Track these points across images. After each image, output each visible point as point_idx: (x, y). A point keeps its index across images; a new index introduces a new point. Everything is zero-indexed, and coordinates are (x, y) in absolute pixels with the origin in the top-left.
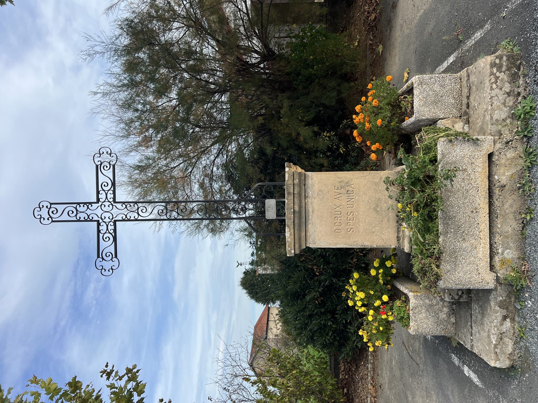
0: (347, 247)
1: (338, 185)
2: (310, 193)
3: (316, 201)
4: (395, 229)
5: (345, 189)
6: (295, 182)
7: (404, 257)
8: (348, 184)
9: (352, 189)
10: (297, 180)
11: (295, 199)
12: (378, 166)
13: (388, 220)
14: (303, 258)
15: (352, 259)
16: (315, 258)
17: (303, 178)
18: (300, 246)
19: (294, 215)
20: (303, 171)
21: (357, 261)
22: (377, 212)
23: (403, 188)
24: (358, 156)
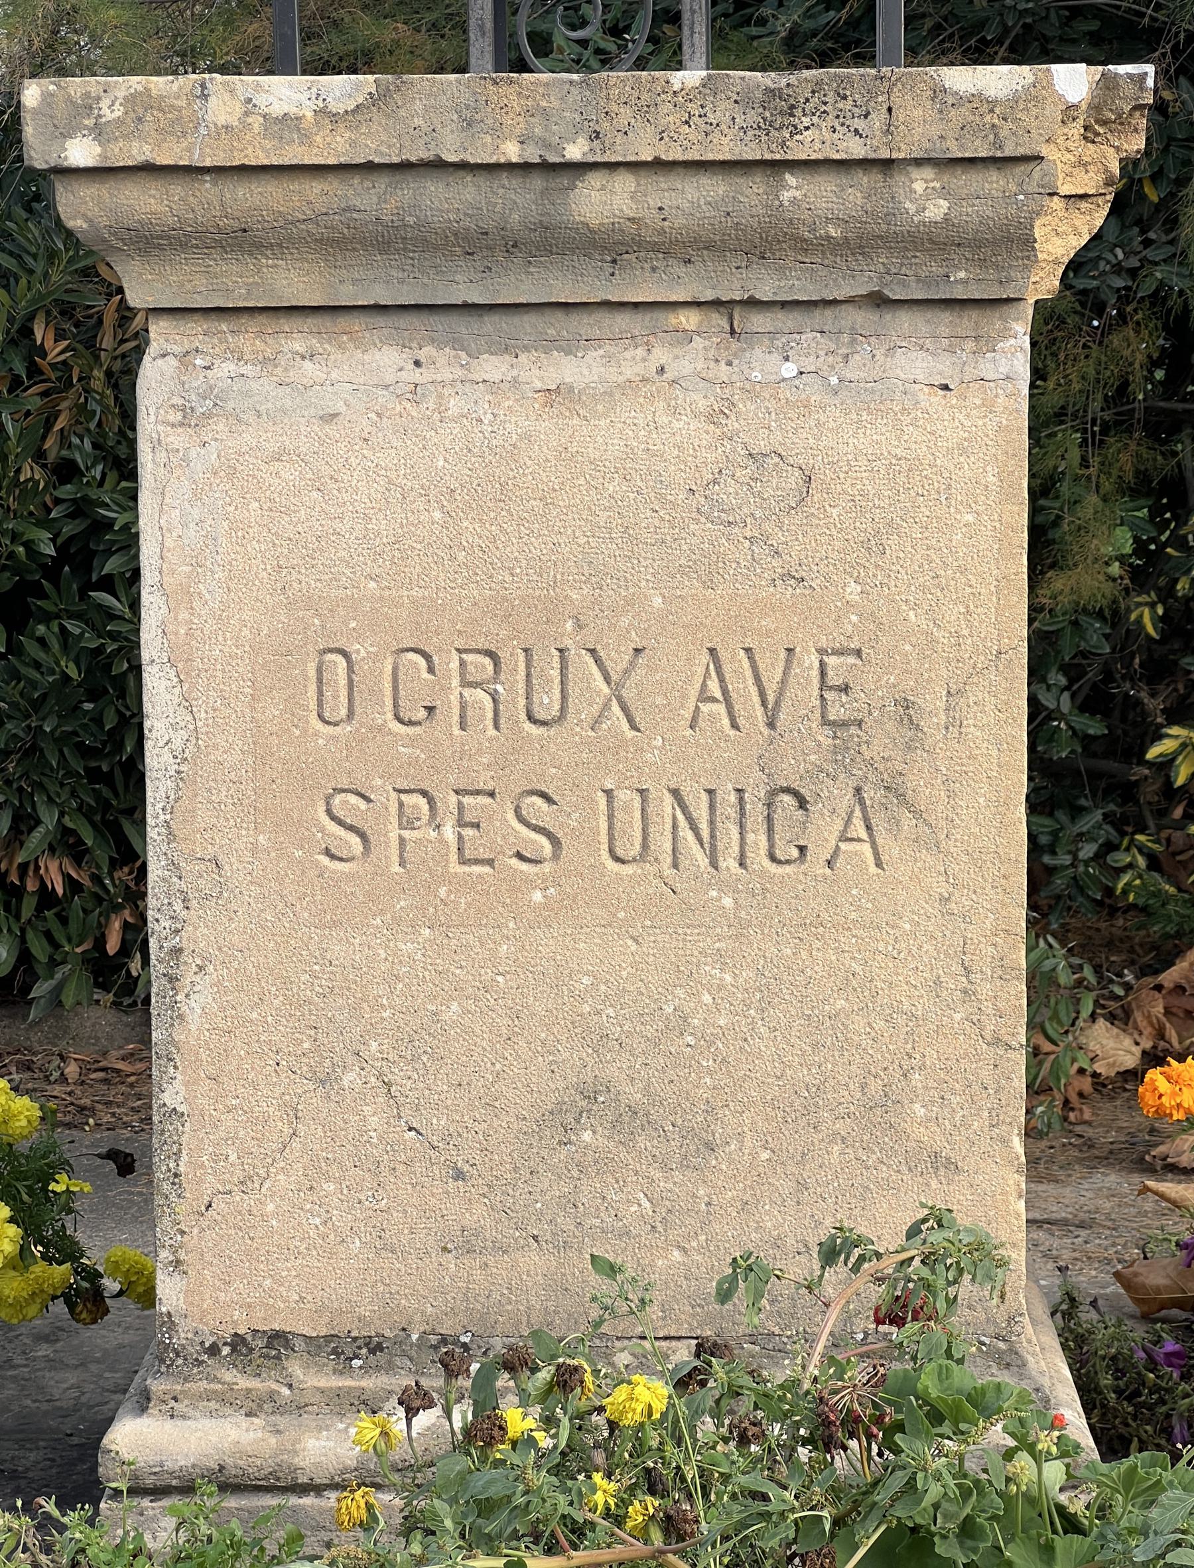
0: (157, 791)
1: (874, 686)
2: (781, 363)
3: (689, 428)
4: (365, 1313)
5: (823, 771)
6: (921, 181)
7: (64, 1385)
8: (884, 800)
9: (819, 854)
10: (937, 210)
11: (714, 188)
12: (1074, 1120)
13: (466, 1244)
14: (55, 351)
15: (68, 845)
16: (66, 471)
17: (963, 280)
18: (151, 242)
19: (525, 167)
20: (1044, 282)
21: (46, 897)
22: (562, 1121)
23: (852, 1425)
24: (1109, 905)
